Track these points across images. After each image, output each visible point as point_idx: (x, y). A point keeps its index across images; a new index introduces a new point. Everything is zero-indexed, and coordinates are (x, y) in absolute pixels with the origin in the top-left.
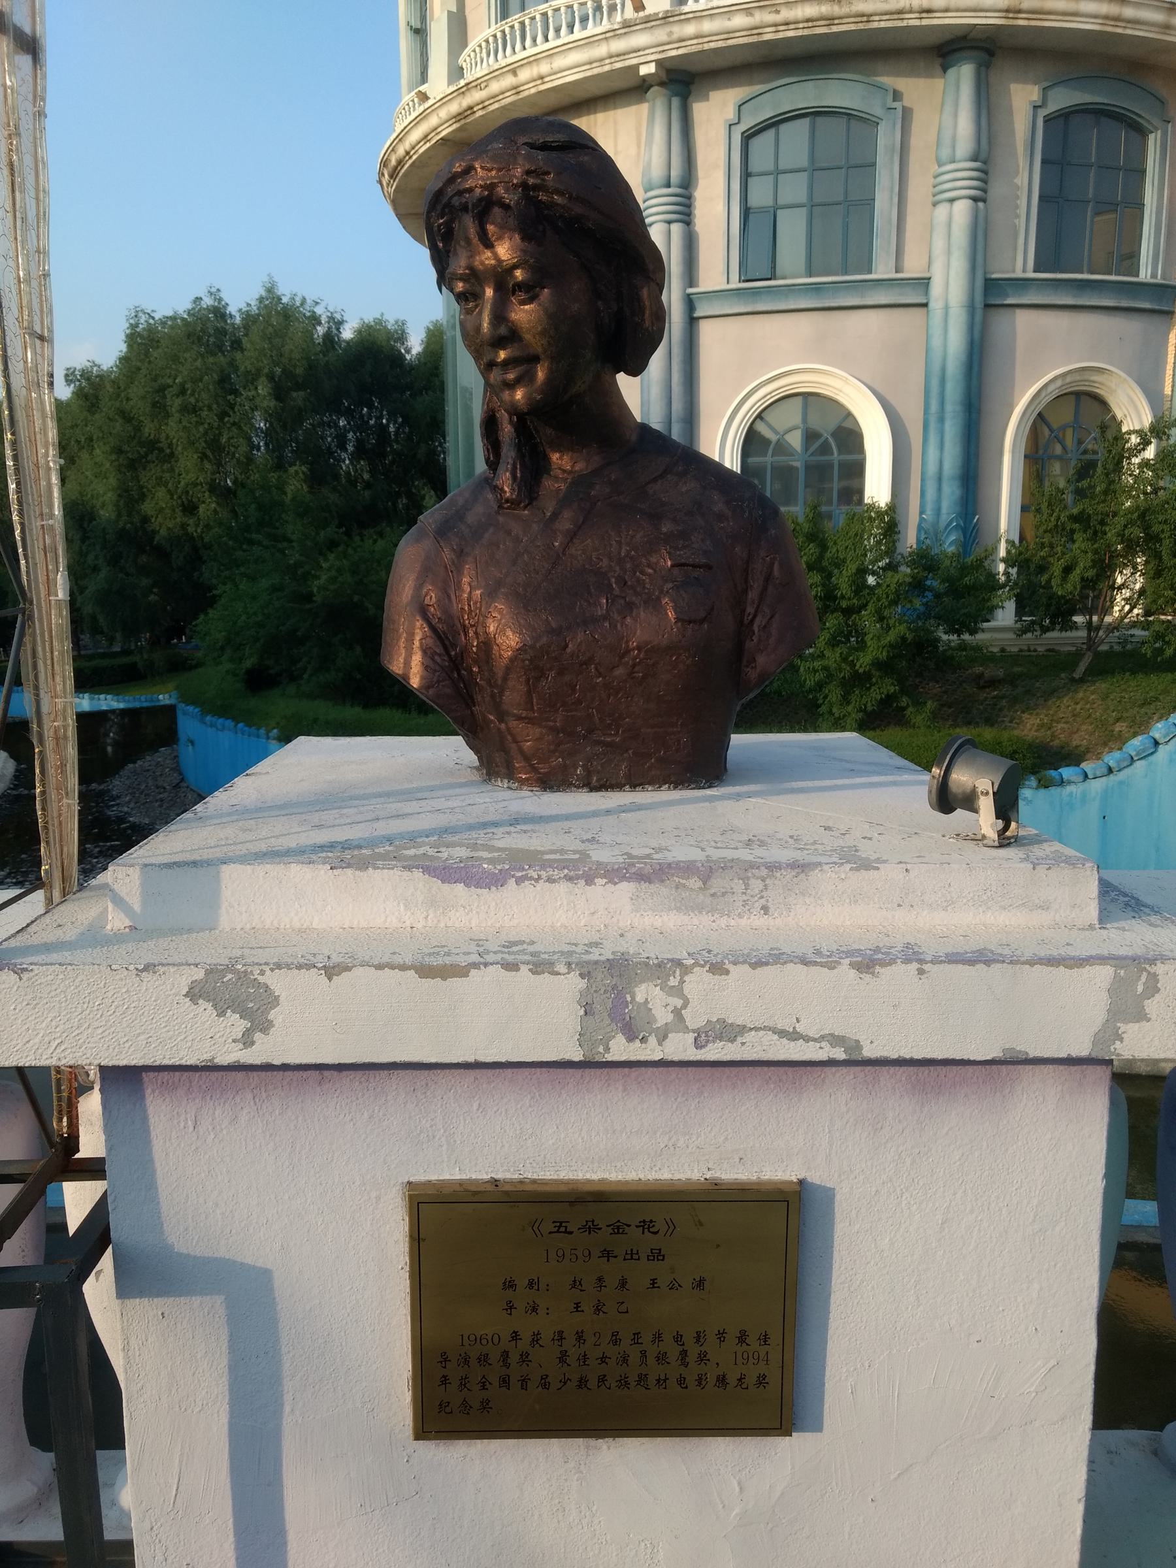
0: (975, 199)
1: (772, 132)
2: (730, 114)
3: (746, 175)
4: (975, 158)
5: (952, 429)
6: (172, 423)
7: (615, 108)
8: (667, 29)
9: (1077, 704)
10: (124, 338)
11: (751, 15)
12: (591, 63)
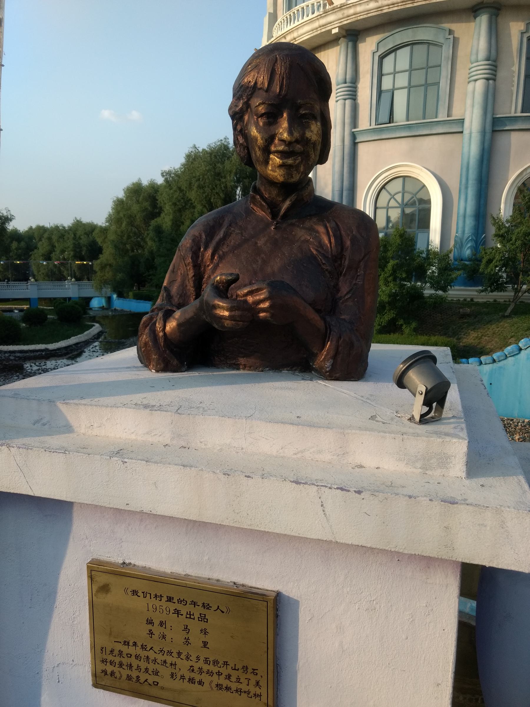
0: (487, 79)
2: (374, 48)
3: (381, 75)
4: (488, 59)
5: (471, 192)
6: (193, 192)
7: (328, 49)
8: (342, 12)
9: (498, 328)
10: (185, 156)
12: (313, 30)
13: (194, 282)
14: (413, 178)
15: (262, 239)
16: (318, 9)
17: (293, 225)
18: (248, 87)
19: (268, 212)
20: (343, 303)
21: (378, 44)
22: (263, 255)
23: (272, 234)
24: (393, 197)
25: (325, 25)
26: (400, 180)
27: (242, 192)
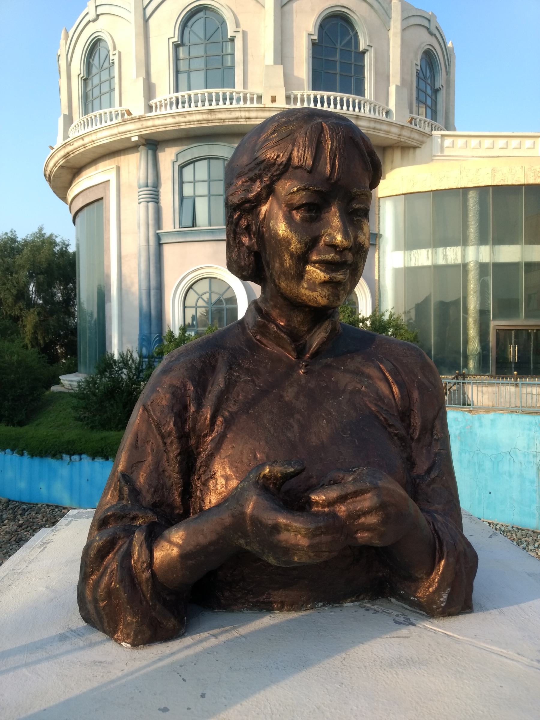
1: (192, 165)
2: (173, 158)
3: (181, 183)
7: (128, 154)
8: (141, 123)
11: (175, 118)
12: (112, 136)
13: (180, 463)
14: (219, 279)
15: (290, 390)
16: (116, 117)
17: (328, 366)
18: (274, 164)
19: (290, 348)
20: (429, 485)
21: (177, 155)
22: (297, 416)
23: (303, 381)
24: (200, 297)
25: (125, 132)
26: (206, 282)
27: (36, 288)
